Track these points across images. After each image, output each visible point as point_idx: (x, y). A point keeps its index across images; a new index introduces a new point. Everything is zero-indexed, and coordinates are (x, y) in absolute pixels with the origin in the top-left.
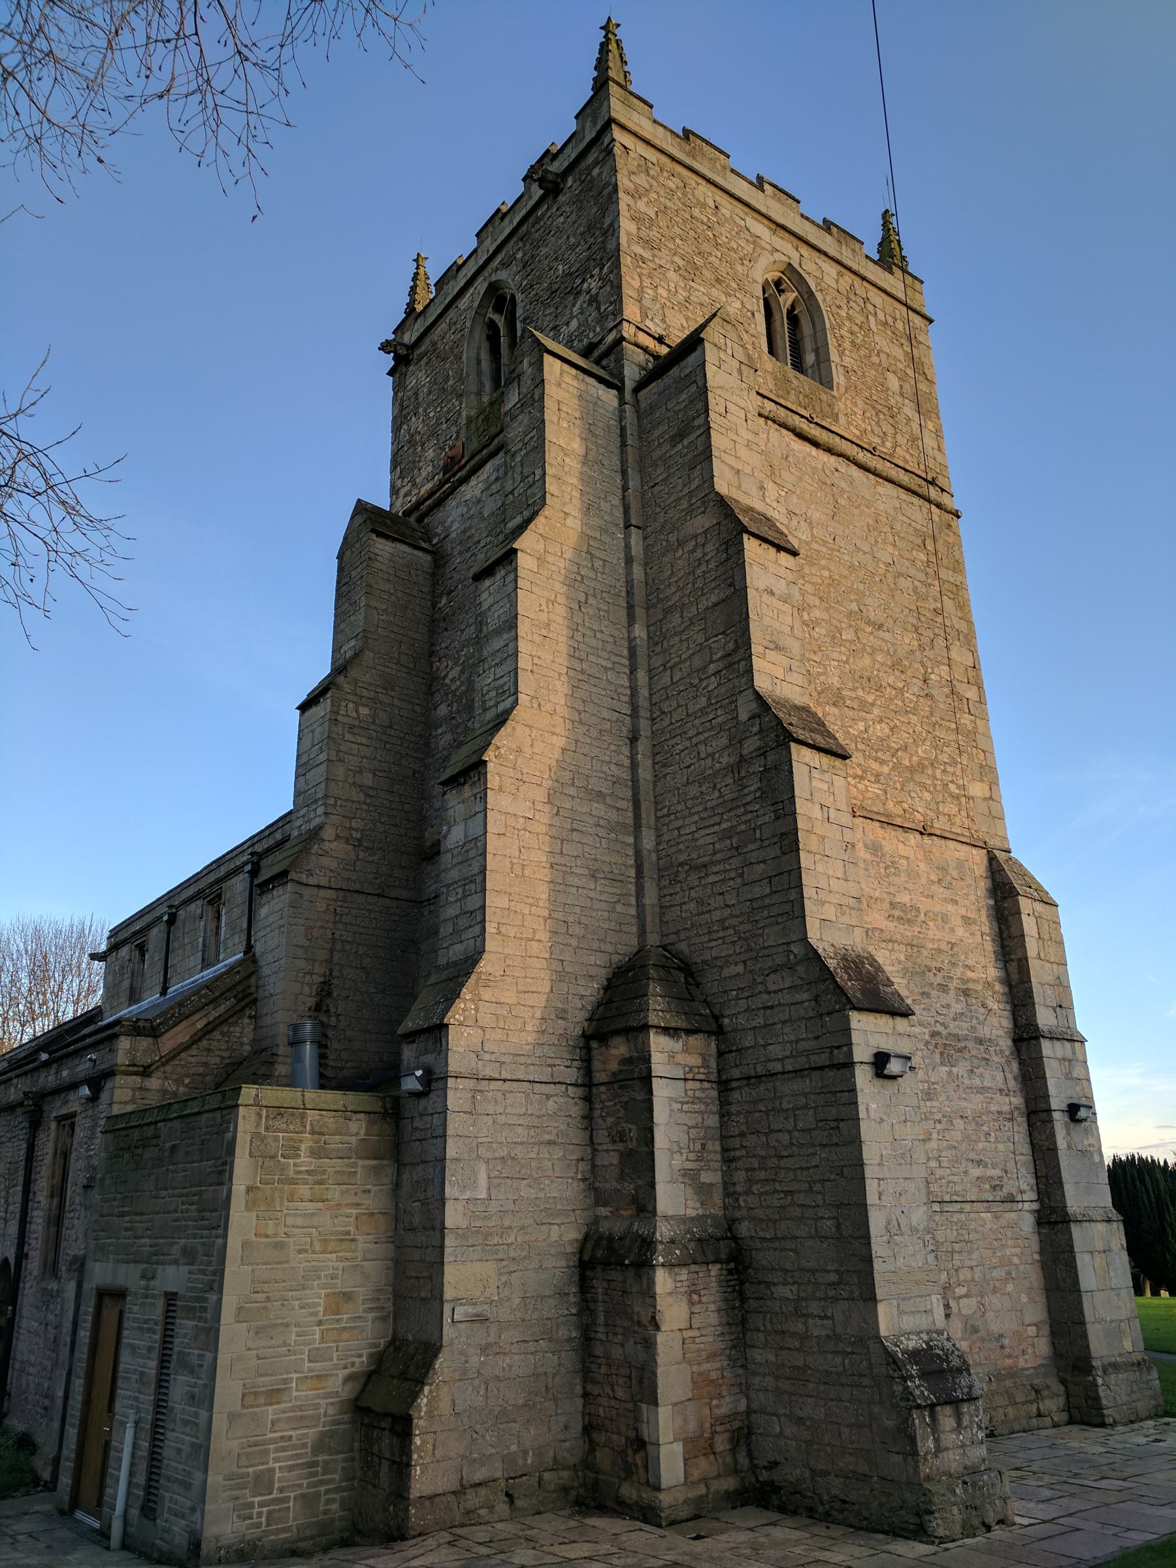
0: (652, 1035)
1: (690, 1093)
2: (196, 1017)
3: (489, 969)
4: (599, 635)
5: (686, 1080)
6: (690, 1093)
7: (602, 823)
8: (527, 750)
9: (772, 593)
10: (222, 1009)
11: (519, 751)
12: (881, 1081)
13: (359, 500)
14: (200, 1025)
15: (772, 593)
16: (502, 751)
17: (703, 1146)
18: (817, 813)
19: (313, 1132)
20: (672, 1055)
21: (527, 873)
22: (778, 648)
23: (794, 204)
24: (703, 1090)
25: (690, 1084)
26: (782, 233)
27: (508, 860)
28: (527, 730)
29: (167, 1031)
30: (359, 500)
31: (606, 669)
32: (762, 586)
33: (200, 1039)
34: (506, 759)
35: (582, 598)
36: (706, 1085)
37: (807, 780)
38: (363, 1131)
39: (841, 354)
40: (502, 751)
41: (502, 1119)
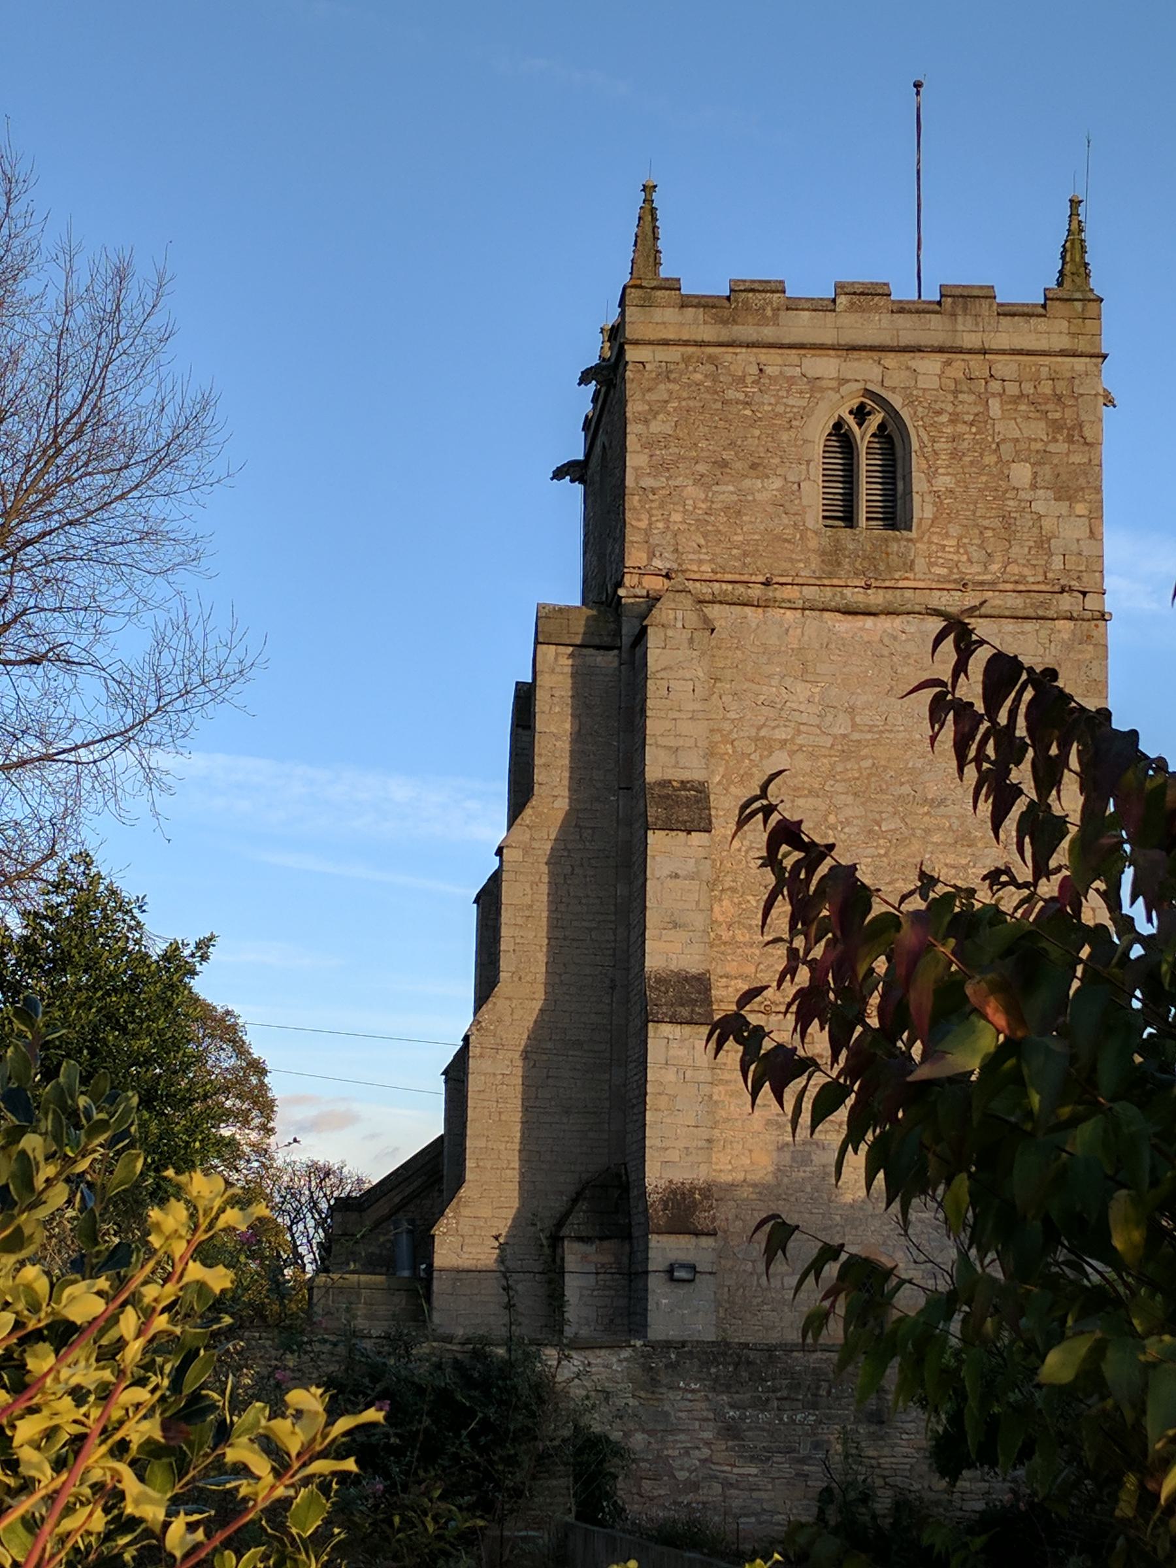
0: (566, 1243)
1: (601, 1283)
2: (393, 1193)
3: (468, 1193)
4: (584, 901)
5: (597, 1273)
6: (601, 1283)
7: (578, 1067)
8: (507, 1019)
9: (677, 876)
10: (416, 1184)
11: (500, 1021)
12: (674, 1285)
13: (517, 683)
14: (397, 1200)
15: (677, 876)
16: (483, 1024)
17: (612, 1321)
18: (670, 1076)
19: (365, 1303)
20: (585, 1257)
21: (503, 1118)
22: (676, 925)
23: (882, 302)
24: (613, 1280)
25: (601, 1277)
26: (856, 354)
27: (486, 1110)
28: (508, 1002)
29: (369, 1207)
30: (517, 683)
31: (590, 930)
32: (666, 872)
33: (397, 1211)
34: (487, 1030)
35: (568, 870)
36: (618, 1276)
37: (664, 1049)
38: (404, 1302)
39: (930, 477)
40: (483, 1024)
41: (478, 1298)
